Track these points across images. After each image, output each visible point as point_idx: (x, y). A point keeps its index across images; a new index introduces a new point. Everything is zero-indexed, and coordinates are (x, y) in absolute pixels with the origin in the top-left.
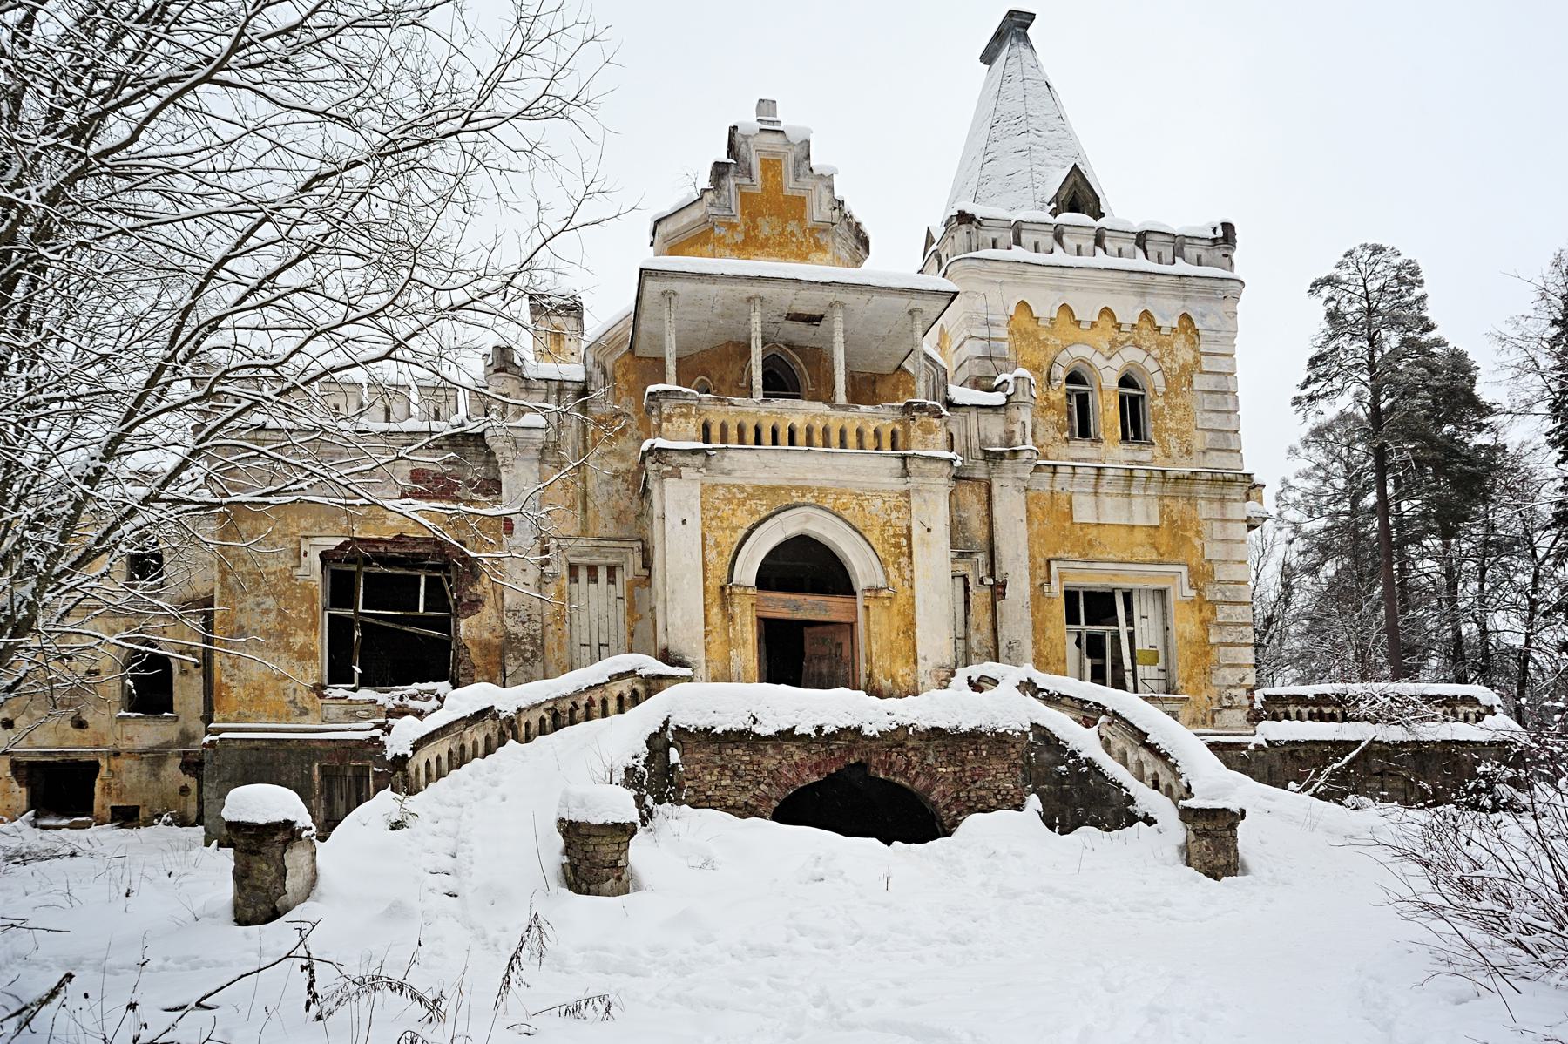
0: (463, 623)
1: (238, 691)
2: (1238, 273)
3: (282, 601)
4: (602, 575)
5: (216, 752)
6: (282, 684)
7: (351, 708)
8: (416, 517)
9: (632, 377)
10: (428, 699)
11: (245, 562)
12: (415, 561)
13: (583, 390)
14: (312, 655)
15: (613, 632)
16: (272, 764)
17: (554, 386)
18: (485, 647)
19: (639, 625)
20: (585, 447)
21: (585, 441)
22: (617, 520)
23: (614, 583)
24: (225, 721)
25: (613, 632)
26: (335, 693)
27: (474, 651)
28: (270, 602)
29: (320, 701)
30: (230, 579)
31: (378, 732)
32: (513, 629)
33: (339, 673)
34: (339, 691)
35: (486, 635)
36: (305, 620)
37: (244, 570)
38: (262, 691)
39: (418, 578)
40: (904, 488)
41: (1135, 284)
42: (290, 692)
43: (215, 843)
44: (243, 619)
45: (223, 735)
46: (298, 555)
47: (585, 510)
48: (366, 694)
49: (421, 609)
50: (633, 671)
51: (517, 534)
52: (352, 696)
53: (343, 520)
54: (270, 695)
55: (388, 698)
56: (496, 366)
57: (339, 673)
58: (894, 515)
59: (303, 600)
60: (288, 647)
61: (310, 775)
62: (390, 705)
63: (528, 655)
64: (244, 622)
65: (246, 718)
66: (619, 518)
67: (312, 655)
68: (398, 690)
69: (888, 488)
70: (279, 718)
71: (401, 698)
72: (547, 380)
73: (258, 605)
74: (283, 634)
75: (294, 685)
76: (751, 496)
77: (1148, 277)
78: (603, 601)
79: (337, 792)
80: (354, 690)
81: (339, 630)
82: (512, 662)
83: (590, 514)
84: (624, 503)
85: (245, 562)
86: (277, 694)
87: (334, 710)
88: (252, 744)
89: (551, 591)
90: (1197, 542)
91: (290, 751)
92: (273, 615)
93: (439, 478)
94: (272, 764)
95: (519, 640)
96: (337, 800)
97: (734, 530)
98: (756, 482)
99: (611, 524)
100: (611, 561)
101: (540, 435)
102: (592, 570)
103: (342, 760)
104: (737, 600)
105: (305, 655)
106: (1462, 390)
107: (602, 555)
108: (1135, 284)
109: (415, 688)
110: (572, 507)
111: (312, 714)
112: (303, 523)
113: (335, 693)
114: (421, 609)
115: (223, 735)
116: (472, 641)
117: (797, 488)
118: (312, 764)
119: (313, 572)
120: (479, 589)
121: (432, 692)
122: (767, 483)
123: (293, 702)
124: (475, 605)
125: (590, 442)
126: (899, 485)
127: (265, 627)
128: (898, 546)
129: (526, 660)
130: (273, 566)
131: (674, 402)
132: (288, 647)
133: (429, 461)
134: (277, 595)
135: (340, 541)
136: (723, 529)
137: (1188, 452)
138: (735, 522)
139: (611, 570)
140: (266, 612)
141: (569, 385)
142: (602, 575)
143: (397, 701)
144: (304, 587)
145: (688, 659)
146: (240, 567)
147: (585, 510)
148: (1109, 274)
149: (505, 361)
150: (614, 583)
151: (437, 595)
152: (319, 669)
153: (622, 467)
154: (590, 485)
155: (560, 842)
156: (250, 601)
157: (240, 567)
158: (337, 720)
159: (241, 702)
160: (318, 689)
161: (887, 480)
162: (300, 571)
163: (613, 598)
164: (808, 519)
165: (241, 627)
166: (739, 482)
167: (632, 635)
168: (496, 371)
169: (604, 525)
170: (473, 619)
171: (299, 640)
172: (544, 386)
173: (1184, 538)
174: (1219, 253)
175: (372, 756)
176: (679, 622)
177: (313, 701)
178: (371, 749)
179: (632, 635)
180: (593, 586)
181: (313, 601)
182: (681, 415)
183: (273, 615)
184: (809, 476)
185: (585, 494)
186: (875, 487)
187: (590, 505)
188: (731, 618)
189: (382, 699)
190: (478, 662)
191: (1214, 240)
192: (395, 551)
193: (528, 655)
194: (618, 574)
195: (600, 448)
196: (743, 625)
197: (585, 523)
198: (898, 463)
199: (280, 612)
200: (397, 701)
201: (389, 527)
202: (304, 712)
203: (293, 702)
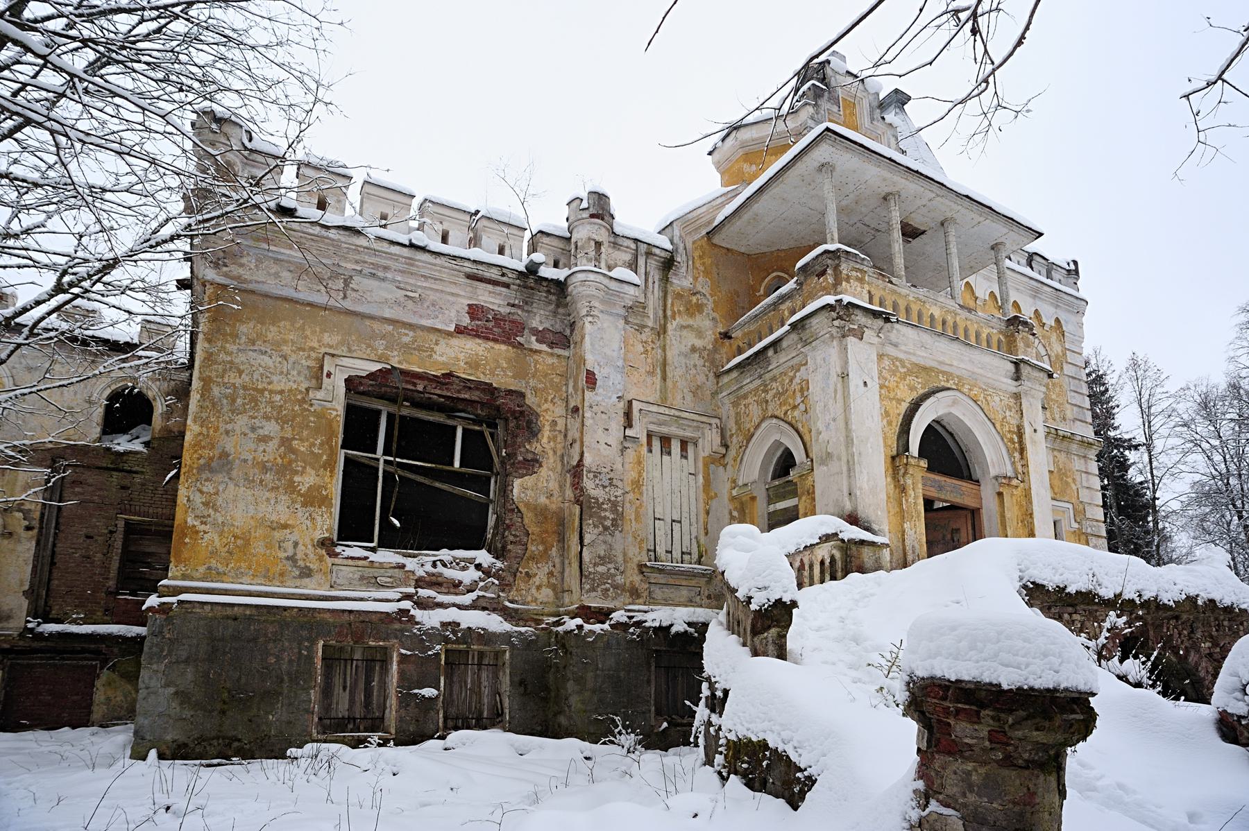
0: (517, 483)
1: (211, 538)
2: (1081, 294)
3: (287, 428)
4: (676, 447)
5: (169, 620)
6: (278, 535)
7: (370, 572)
8: (458, 356)
9: (708, 261)
10: (464, 569)
11: (240, 372)
12: (450, 407)
13: (668, 264)
14: (325, 501)
15: (685, 509)
16: (255, 640)
17: (643, 248)
18: (542, 513)
19: (714, 503)
20: (665, 316)
21: (665, 311)
22: (694, 394)
23: (686, 458)
24: (184, 577)
25: (685, 509)
26: (349, 552)
27: (529, 518)
28: (271, 428)
29: (329, 560)
30: (216, 391)
31: (406, 604)
32: (593, 493)
33: (353, 525)
34: (355, 550)
35: (543, 500)
36: (317, 457)
37: (238, 382)
38: (247, 543)
39: (455, 428)
40: (1015, 390)
41: (1032, 289)
42: (289, 546)
43: (153, 753)
44: (229, 445)
45: (183, 597)
46: (318, 375)
47: (664, 379)
48: (387, 556)
49: (457, 464)
50: (836, 534)
51: (599, 390)
52: (373, 557)
53: (380, 345)
54: (258, 548)
55: (420, 563)
56: (592, 211)
57: (353, 525)
58: (1008, 413)
59: (317, 431)
60: (291, 488)
61: (310, 659)
62: (420, 573)
63: (608, 523)
64: (229, 448)
65: (220, 576)
66: (696, 391)
67: (325, 501)
68: (428, 557)
69: (1004, 387)
70: (269, 579)
71: (434, 565)
72: (636, 240)
73: (253, 429)
74: (285, 470)
75: (293, 538)
76: (910, 372)
77: (1039, 285)
78: (676, 475)
79: (337, 681)
80: (373, 550)
81: (357, 479)
82: (591, 529)
83: (669, 383)
84: (701, 379)
85: (240, 372)
86: (269, 546)
87: (347, 572)
88: (229, 611)
89: (631, 455)
90: (1074, 487)
91: (284, 625)
92: (272, 445)
93: (498, 319)
94: (255, 640)
95: (600, 506)
96: (338, 690)
97: (899, 401)
98: (914, 359)
99: (689, 397)
100: (688, 434)
101: (632, 291)
102: (666, 441)
103: (358, 638)
104: (911, 471)
105: (314, 499)
106: (167, 569)
107: (680, 426)
108: (1032, 289)
109: (445, 554)
110: (651, 373)
111: (317, 577)
112: (327, 338)
113: (349, 552)
114: (457, 464)
115: (183, 597)
116: (527, 505)
117: (944, 373)
118: (313, 642)
119: (333, 400)
120: (535, 447)
121: (471, 561)
122: (923, 363)
123: (292, 559)
124: (532, 464)
125: (669, 313)
126: (1011, 386)
127: (261, 458)
128: (1011, 440)
129: (606, 528)
130: (279, 383)
131: (852, 264)
132: (291, 488)
133: (494, 300)
134: (282, 421)
135: (378, 367)
136: (891, 399)
137: (1064, 419)
138: (899, 395)
139: (684, 444)
140: (265, 439)
141: (657, 251)
142: (676, 447)
143: (429, 568)
144: (320, 415)
145: (875, 527)
146: (232, 377)
147: (664, 379)
148: (1019, 276)
149: (603, 209)
150: (686, 458)
151: (476, 450)
152: (328, 521)
153: (699, 343)
154: (669, 354)
155: (906, 734)
156: (242, 422)
157: (232, 377)
158: (350, 585)
159: (214, 553)
160: (327, 545)
161: (1005, 380)
162: (320, 395)
163: (685, 473)
164: (955, 403)
165: (224, 455)
166: (901, 356)
167: (708, 513)
168: (592, 216)
169: (681, 399)
170: (529, 480)
171: (307, 480)
172: (633, 246)
173: (1067, 483)
174: (1071, 281)
175: (398, 635)
176: (865, 486)
177: (321, 559)
178: (397, 626)
179: (708, 513)
180: (666, 458)
181: (332, 434)
182: (858, 279)
183: (272, 445)
184: (955, 363)
185: (664, 364)
186: (997, 384)
187: (669, 375)
188: (903, 490)
189: (411, 564)
190: (532, 529)
191: (1069, 271)
192: (436, 392)
193: (608, 523)
194: (690, 449)
195: (679, 320)
196: (916, 497)
197: (664, 391)
198: (1011, 367)
199: (285, 442)
200: (429, 568)
201: (436, 362)
202: (306, 573)
203: (292, 559)
